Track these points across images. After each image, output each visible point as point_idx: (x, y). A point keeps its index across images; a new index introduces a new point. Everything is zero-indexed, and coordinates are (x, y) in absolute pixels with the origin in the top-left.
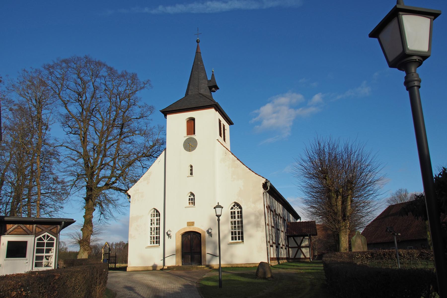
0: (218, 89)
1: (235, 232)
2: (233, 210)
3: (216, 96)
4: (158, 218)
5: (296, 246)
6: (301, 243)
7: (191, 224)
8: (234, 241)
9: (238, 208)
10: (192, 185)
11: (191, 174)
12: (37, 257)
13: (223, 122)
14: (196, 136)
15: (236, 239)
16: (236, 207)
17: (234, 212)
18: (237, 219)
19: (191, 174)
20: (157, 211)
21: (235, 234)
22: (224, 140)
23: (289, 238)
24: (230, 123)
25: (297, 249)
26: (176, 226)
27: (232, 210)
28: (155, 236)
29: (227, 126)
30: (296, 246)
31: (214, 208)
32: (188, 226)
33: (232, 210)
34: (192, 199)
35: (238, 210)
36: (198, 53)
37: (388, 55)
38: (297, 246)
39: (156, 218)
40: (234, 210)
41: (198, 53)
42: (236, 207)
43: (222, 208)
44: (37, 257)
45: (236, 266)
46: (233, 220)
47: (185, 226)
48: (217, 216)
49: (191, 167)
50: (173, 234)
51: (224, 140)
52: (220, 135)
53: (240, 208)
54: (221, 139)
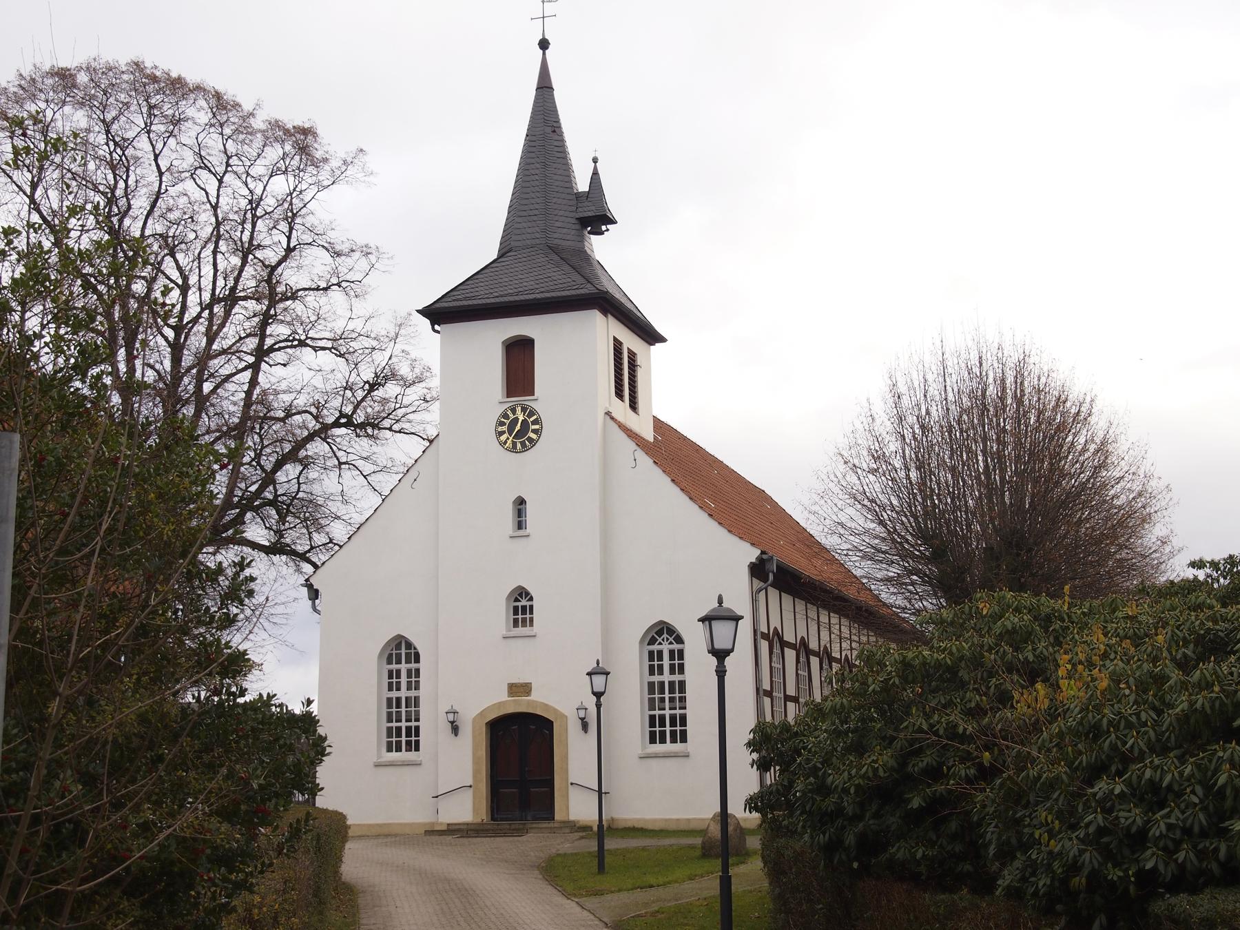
0: (613, 222)
2: (655, 647)
4: (413, 666)
7: (519, 689)
8: (658, 748)
11: (520, 525)
15: (663, 741)
16: (665, 635)
17: (660, 653)
19: (520, 525)
20: (409, 645)
21: (663, 724)
26: (467, 684)
28: (404, 724)
31: (589, 674)
34: (524, 608)
35: (671, 647)
36: (545, 87)
39: (404, 667)
40: (660, 647)
41: (545, 87)
42: (665, 635)
43: (607, 674)
47: (503, 696)
48: (594, 693)
49: (520, 502)
52: (619, 394)
53: (679, 640)
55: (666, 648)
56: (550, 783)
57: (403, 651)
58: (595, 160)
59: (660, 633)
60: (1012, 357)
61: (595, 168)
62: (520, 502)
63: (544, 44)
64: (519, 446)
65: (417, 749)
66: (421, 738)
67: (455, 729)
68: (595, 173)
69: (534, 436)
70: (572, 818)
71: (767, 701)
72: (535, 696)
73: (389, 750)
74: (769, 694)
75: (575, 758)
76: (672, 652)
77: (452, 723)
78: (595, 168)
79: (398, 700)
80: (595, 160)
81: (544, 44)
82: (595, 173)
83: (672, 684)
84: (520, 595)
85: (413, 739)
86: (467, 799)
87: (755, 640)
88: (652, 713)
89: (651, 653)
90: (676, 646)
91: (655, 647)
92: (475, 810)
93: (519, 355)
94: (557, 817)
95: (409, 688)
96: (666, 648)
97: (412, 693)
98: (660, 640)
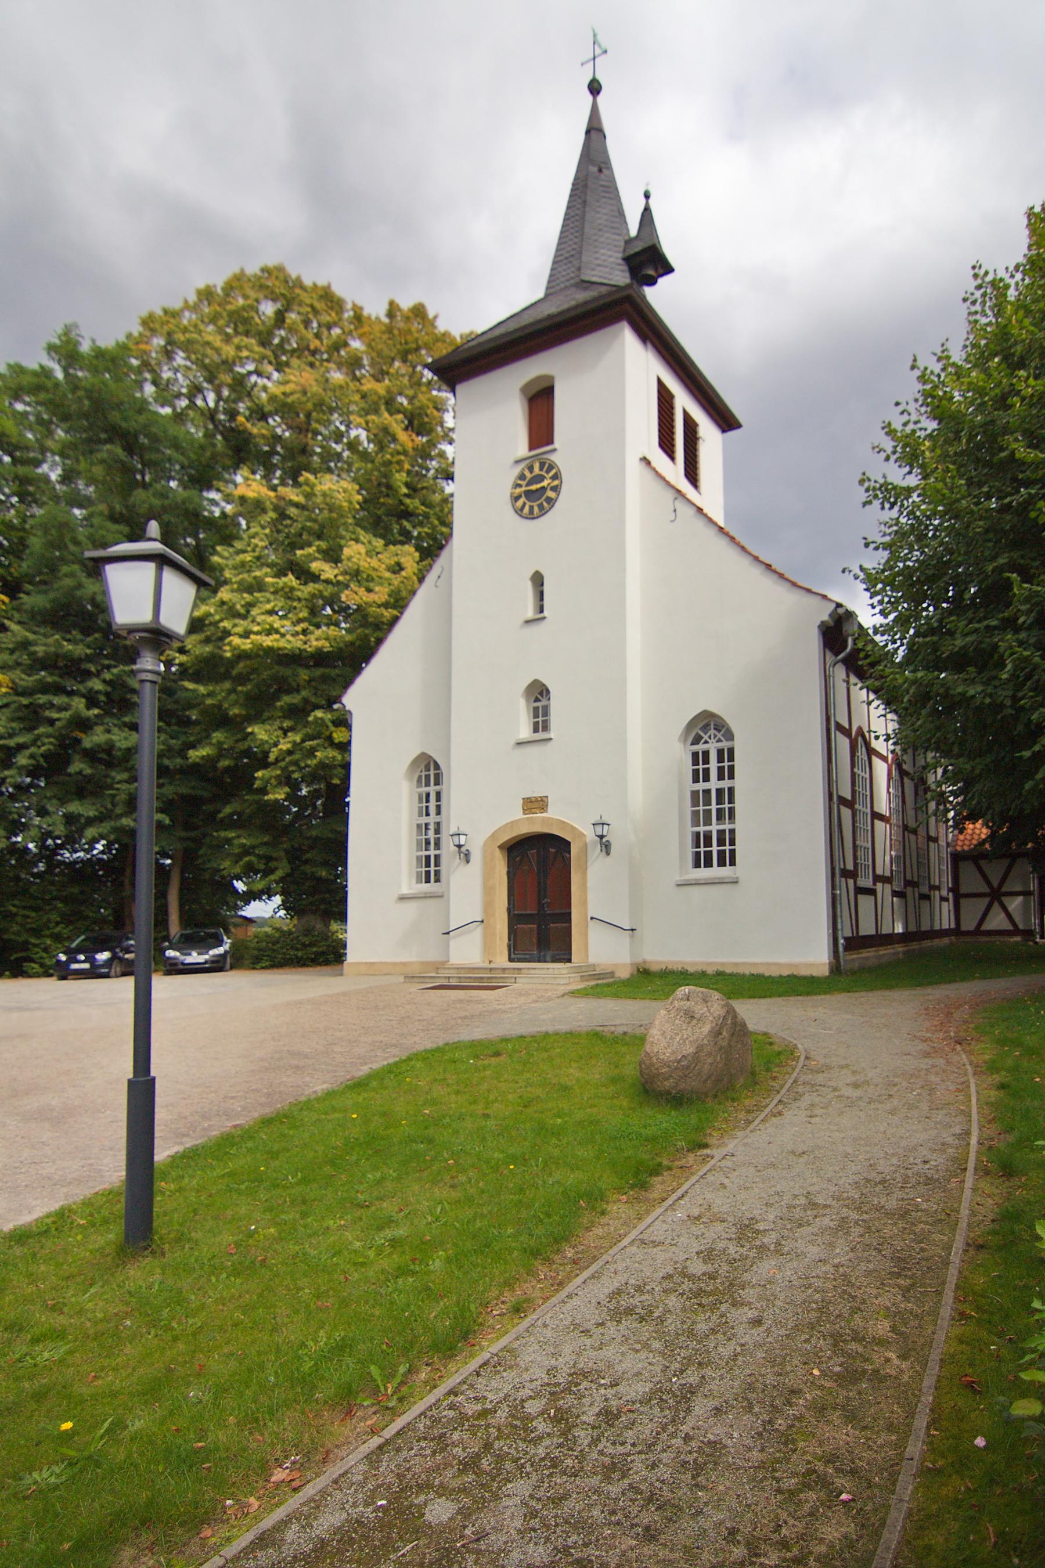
0: (669, 270)
1: (708, 837)
2: (700, 747)
3: (659, 296)
5: (986, 889)
6: (1003, 880)
7: (535, 804)
8: (703, 873)
9: (719, 736)
10: (542, 657)
12: (719, 865)
13: (683, 401)
14: (564, 450)
15: (708, 864)
16: (712, 732)
17: (706, 754)
18: (714, 784)
21: (708, 842)
22: (692, 473)
23: (961, 864)
24: (726, 421)
25: (987, 900)
26: (484, 812)
27: (695, 748)
29: (706, 428)
30: (986, 889)
32: (525, 811)
33: (695, 748)
35: (720, 745)
36: (594, 130)
37: (979, 917)
38: (987, 890)
40: (705, 747)
41: (594, 130)
42: (712, 732)
44: (719, 865)
45: (699, 968)
46: (701, 786)
47: (518, 814)
49: (538, 580)
50: (476, 846)
51: (692, 473)
52: (666, 444)
53: (730, 736)
54: (674, 471)
55: (713, 748)
56: (567, 917)
57: (432, 773)
58: (647, 196)
59: (705, 728)
60: (911, 389)
61: (647, 204)
62: (538, 580)
63: (595, 88)
64: (536, 509)
65: (733, 863)
66: (738, 847)
67: (467, 857)
68: (647, 210)
69: (551, 494)
70: (592, 960)
71: (846, 813)
72: (553, 812)
73: (697, 865)
74: (850, 804)
75: (596, 891)
76: (720, 753)
77: (601, 837)
78: (647, 204)
79: (707, 792)
80: (647, 196)
81: (595, 88)
82: (647, 210)
83: (720, 792)
84: (541, 694)
85: (727, 848)
86: (477, 934)
87: (828, 730)
88: (697, 829)
89: (695, 755)
90: (725, 745)
91: (700, 747)
92: (488, 947)
93: (540, 401)
94: (353, 955)
95: (721, 777)
96: (713, 748)
97: (725, 784)
98: (706, 737)
